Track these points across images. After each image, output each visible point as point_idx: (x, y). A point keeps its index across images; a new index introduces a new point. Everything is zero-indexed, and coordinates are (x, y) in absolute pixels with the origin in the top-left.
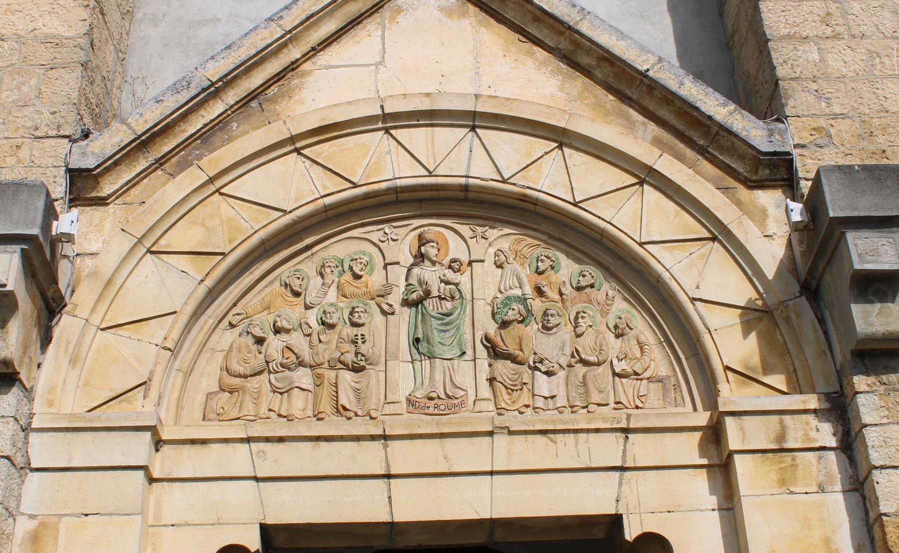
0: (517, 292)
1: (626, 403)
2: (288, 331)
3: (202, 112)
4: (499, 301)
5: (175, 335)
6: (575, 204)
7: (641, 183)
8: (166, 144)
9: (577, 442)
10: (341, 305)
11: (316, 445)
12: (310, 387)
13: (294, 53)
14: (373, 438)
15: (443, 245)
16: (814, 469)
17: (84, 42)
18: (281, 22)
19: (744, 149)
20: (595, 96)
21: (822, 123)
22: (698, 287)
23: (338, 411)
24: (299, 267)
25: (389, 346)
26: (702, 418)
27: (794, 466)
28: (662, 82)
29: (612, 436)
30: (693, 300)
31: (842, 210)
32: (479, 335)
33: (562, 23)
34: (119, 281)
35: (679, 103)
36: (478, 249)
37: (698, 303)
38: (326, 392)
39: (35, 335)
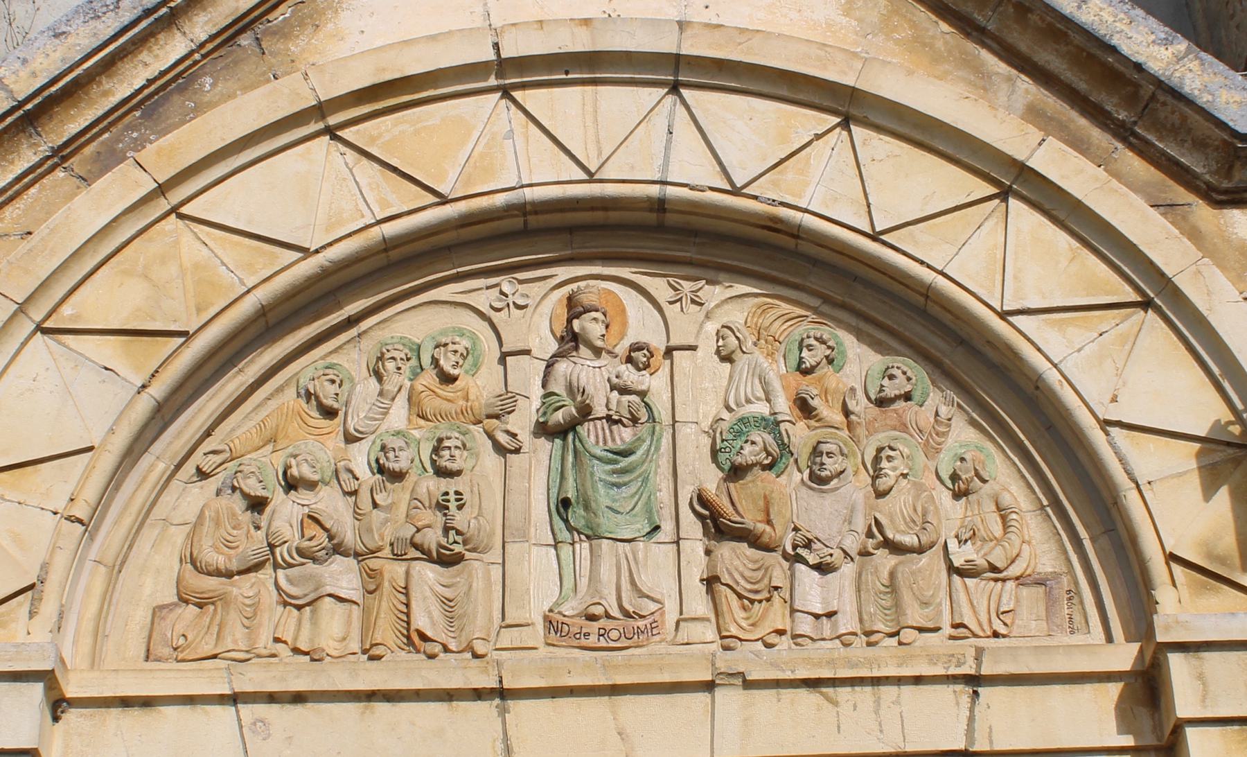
0: (762, 409)
1: (973, 626)
3: (144, 56)
4: (725, 426)
5: (91, 493)
6: (875, 237)
7: (1004, 194)
8: (73, 119)
9: (878, 702)
11: (366, 708)
12: (356, 595)
14: (478, 694)
15: (614, 317)
20: (914, 25)
22: (1114, 399)
23: (410, 642)
26: (1124, 656)
30: (1106, 424)
32: (686, 494)
35: (1078, 39)
36: (684, 324)
37: (1114, 431)
38: (387, 603)
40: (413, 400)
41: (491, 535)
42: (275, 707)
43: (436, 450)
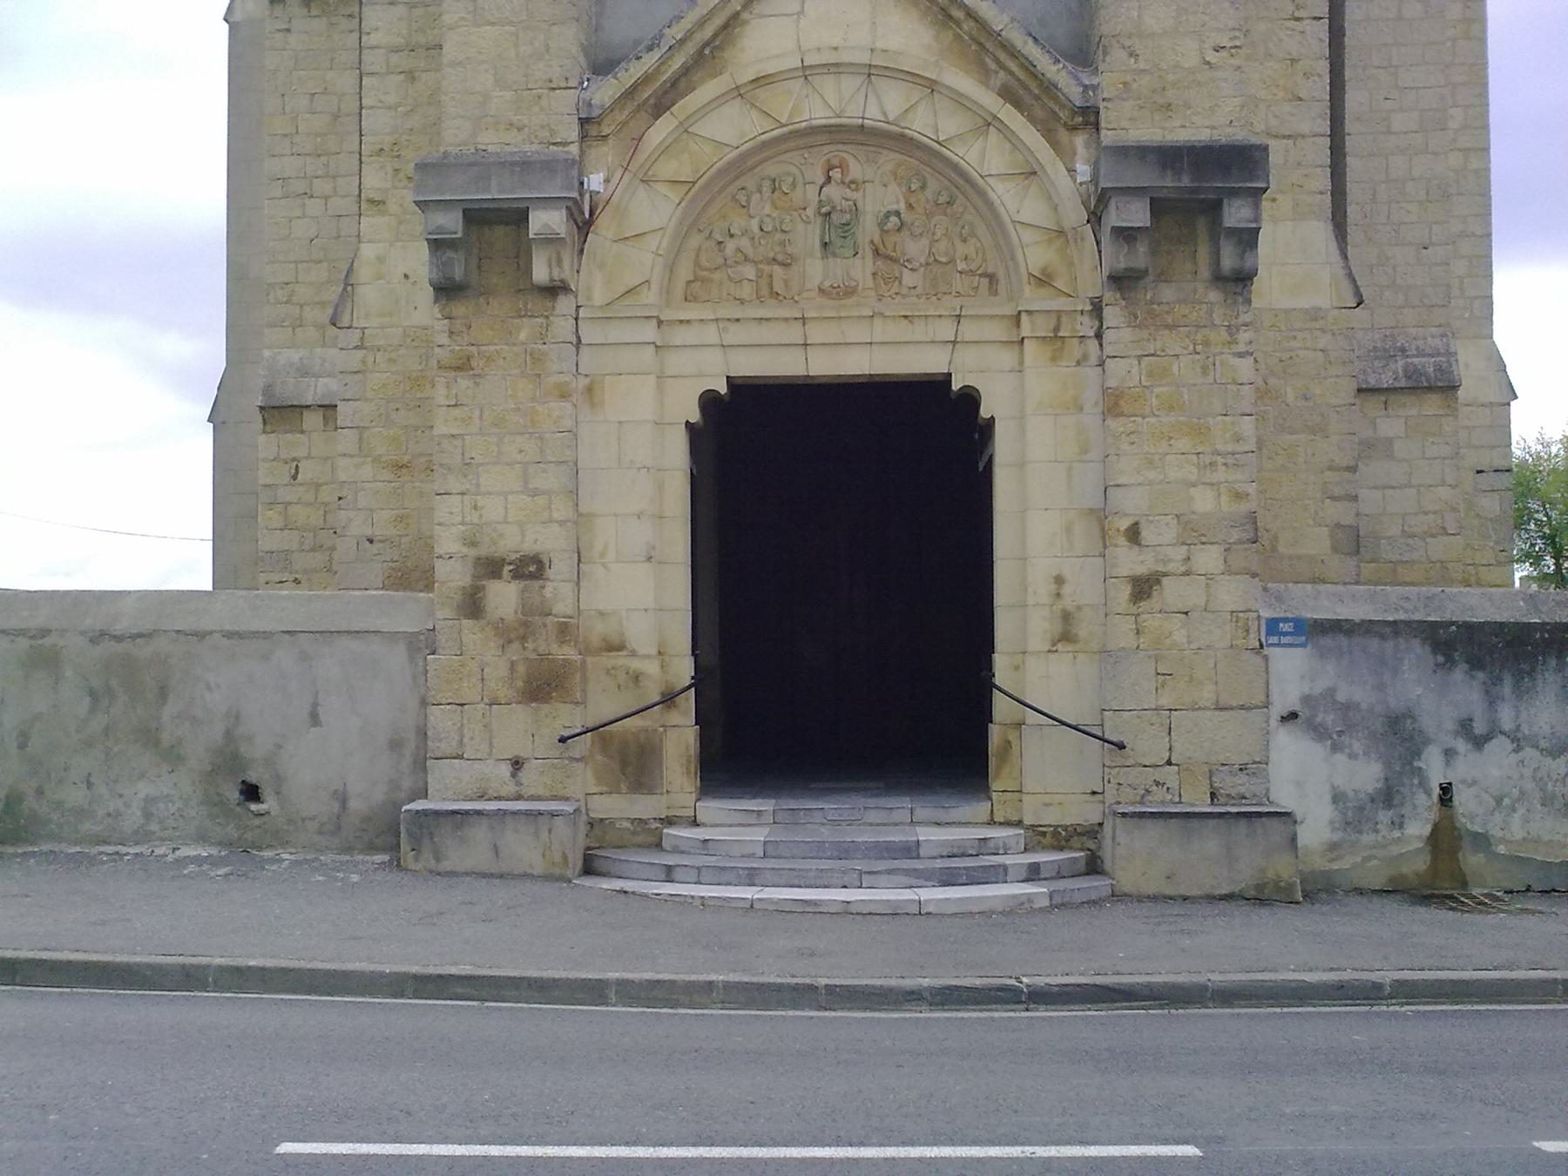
0: (894, 207)
12: (754, 279)
15: (842, 166)
30: (1013, 222)
38: (764, 282)
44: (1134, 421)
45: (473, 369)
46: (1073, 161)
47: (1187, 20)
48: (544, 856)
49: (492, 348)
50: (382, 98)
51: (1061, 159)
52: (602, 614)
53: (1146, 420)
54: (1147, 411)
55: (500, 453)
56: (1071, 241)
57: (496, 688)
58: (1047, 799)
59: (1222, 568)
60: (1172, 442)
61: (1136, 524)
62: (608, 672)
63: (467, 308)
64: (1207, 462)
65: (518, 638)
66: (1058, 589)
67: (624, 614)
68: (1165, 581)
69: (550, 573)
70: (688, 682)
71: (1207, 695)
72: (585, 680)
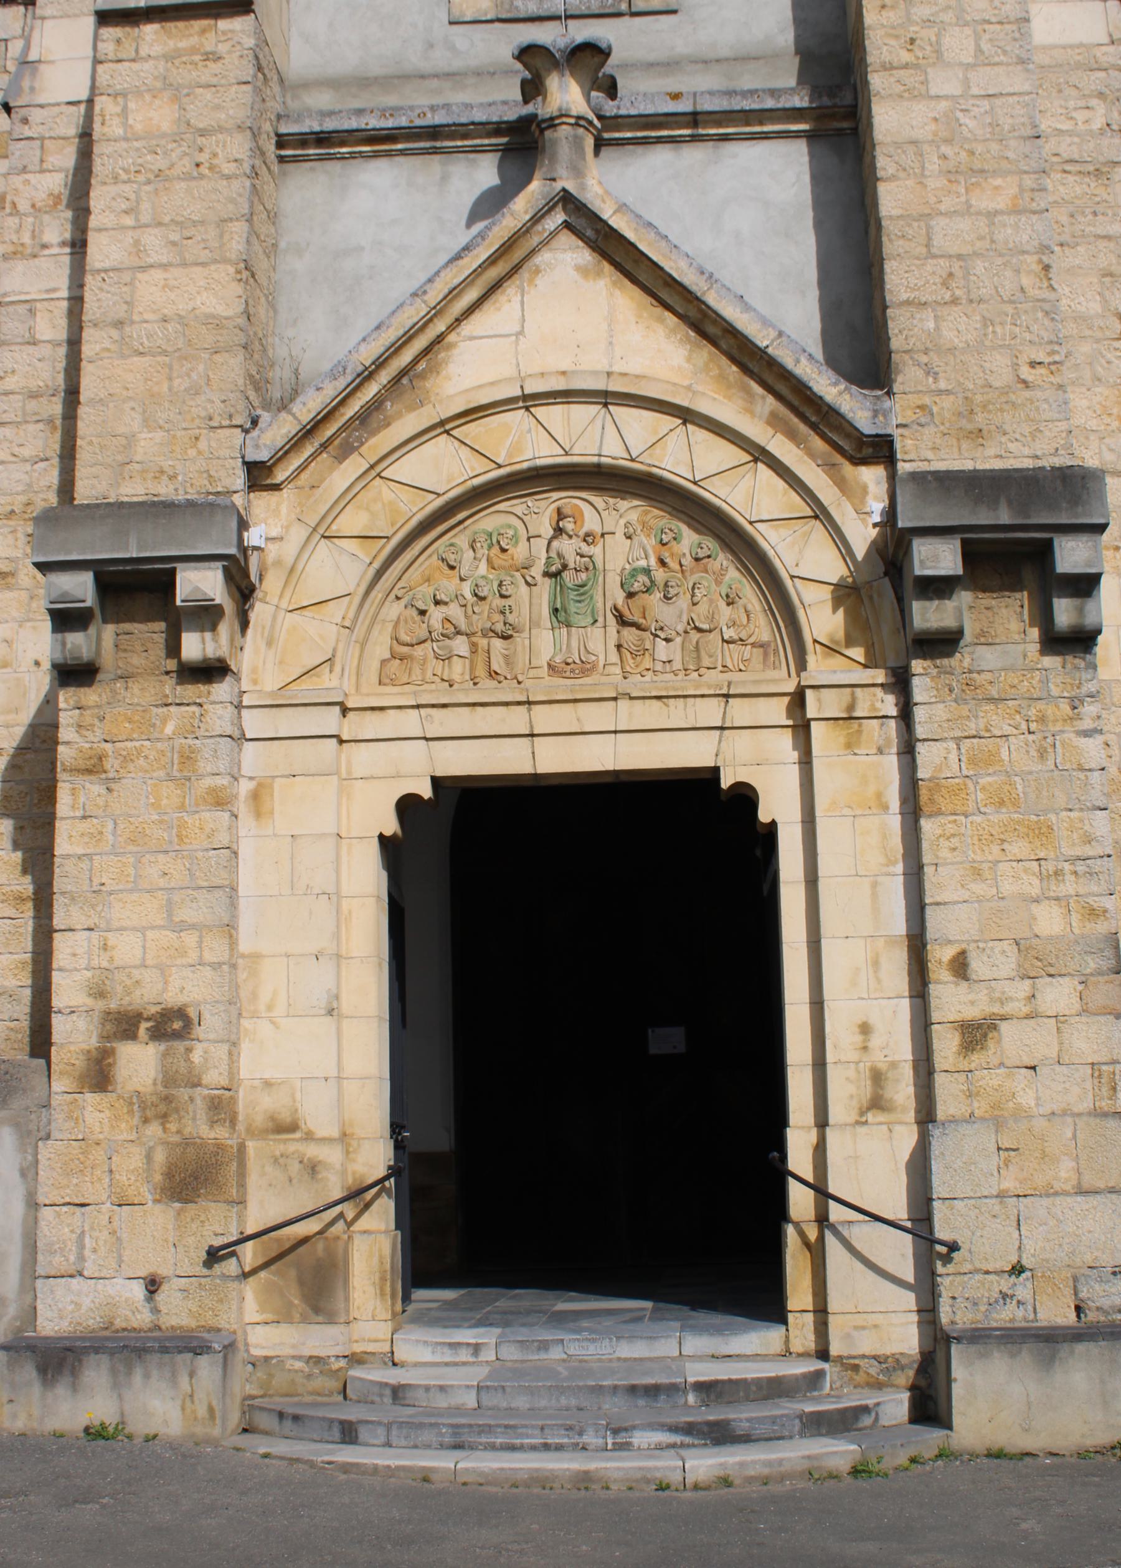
0: (643, 563)
1: (731, 667)
2: (446, 603)
3: (359, 394)
4: (627, 572)
5: (351, 614)
6: (695, 483)
7: (756, 460)
8: (328, 429)
9: (686, 706)
10: (491, 576)
12: (467, 654)
13: (440, 326)
14: (519, 703)
15: (578, 518)
16: (876, 734)
17: (242, 321)
18: (426, 298)
19: (849, 429)
20: (719, 367)
21: (927, 400)
22: (797, 565)
23: (491, 675)
24: (453, 541)
25: (533, 616)
26: (790, 687)
27: (859, 732)
28: (779, 360)
29: (715, 700)
30: (792, 577)
31: (910, 521)
32: (609, 605)
33: (690, 292)
34: (300, 566)
35: (794, 381)
36: (611, 522)
37: (796, 580)
38: (481, 658)
39: (237, 627)
40: (489, 561)
41: (524, 625)
42: (435, 710)
43: (500, 585)
44: (955, 821)
45: (105, 772)
46: (863, 501)
47: (994, 332)
48: (183, 1409)
49: (129, 744)
50: (16, 450)
51: (848, 498)
52: (268, 1084)
53: (970, 819)
54: (971, 807)
55: (138, 876)
56: (866, 601)
57: (127, 1183)
58: (859, 1320)
59: (1077, 1006)
60: (1006, 846)
61: (963, 953)
62: (276, 1160)
63: (100, 695)
64: (1051, 870)
65: (157, 1117)
66: (865, 1041)
67: (298, 1083)
68: (1004, 1026)
69: (198, 1031)
70: (381, 1172)
71: (1065, 1172)
72: (242, 1174)
